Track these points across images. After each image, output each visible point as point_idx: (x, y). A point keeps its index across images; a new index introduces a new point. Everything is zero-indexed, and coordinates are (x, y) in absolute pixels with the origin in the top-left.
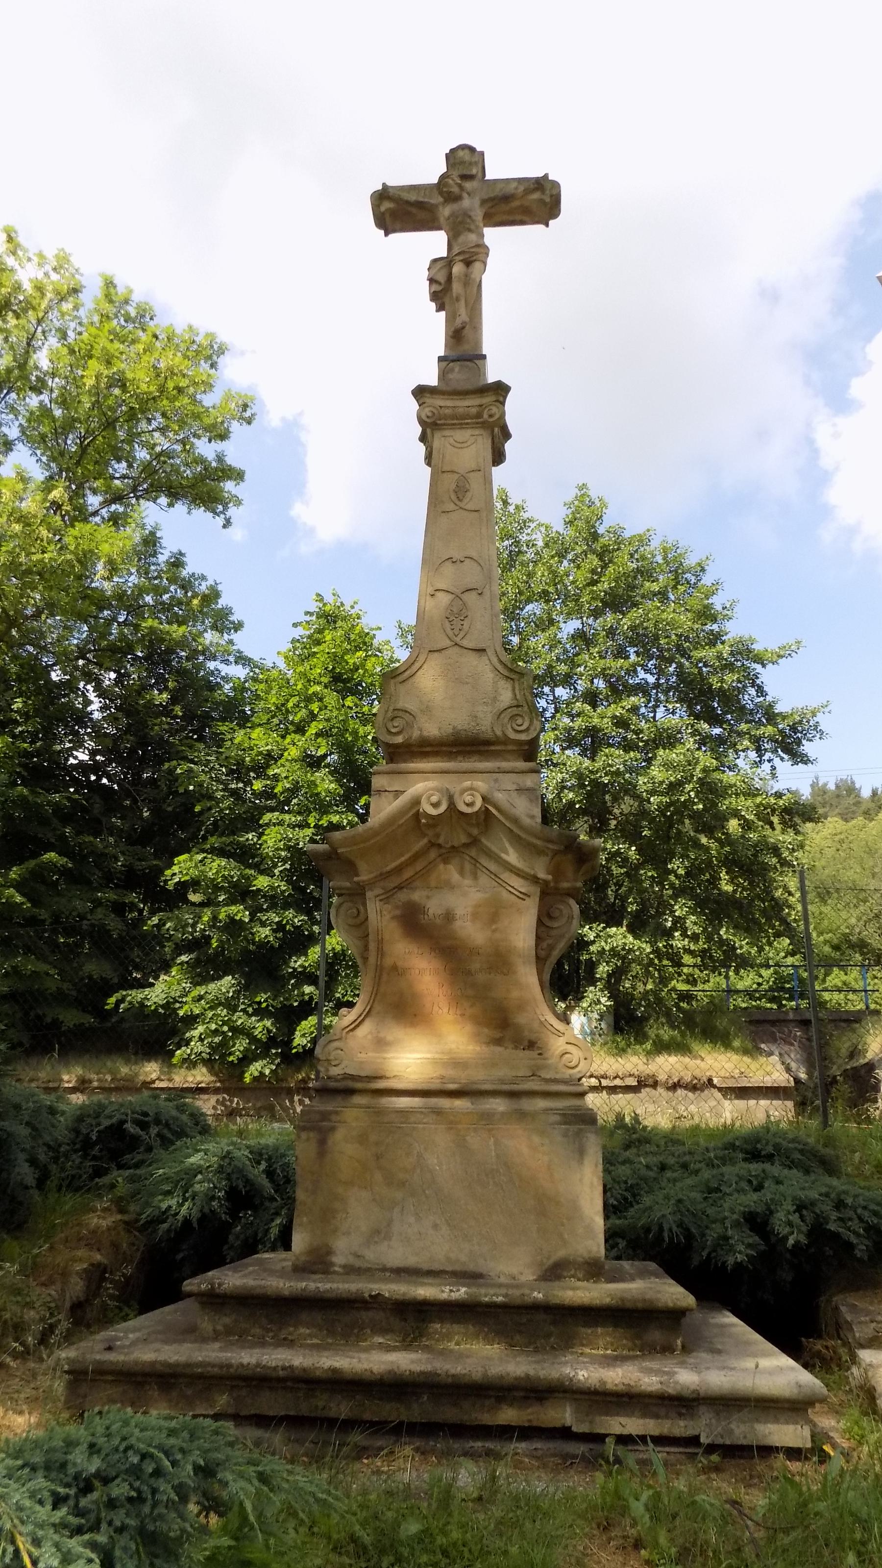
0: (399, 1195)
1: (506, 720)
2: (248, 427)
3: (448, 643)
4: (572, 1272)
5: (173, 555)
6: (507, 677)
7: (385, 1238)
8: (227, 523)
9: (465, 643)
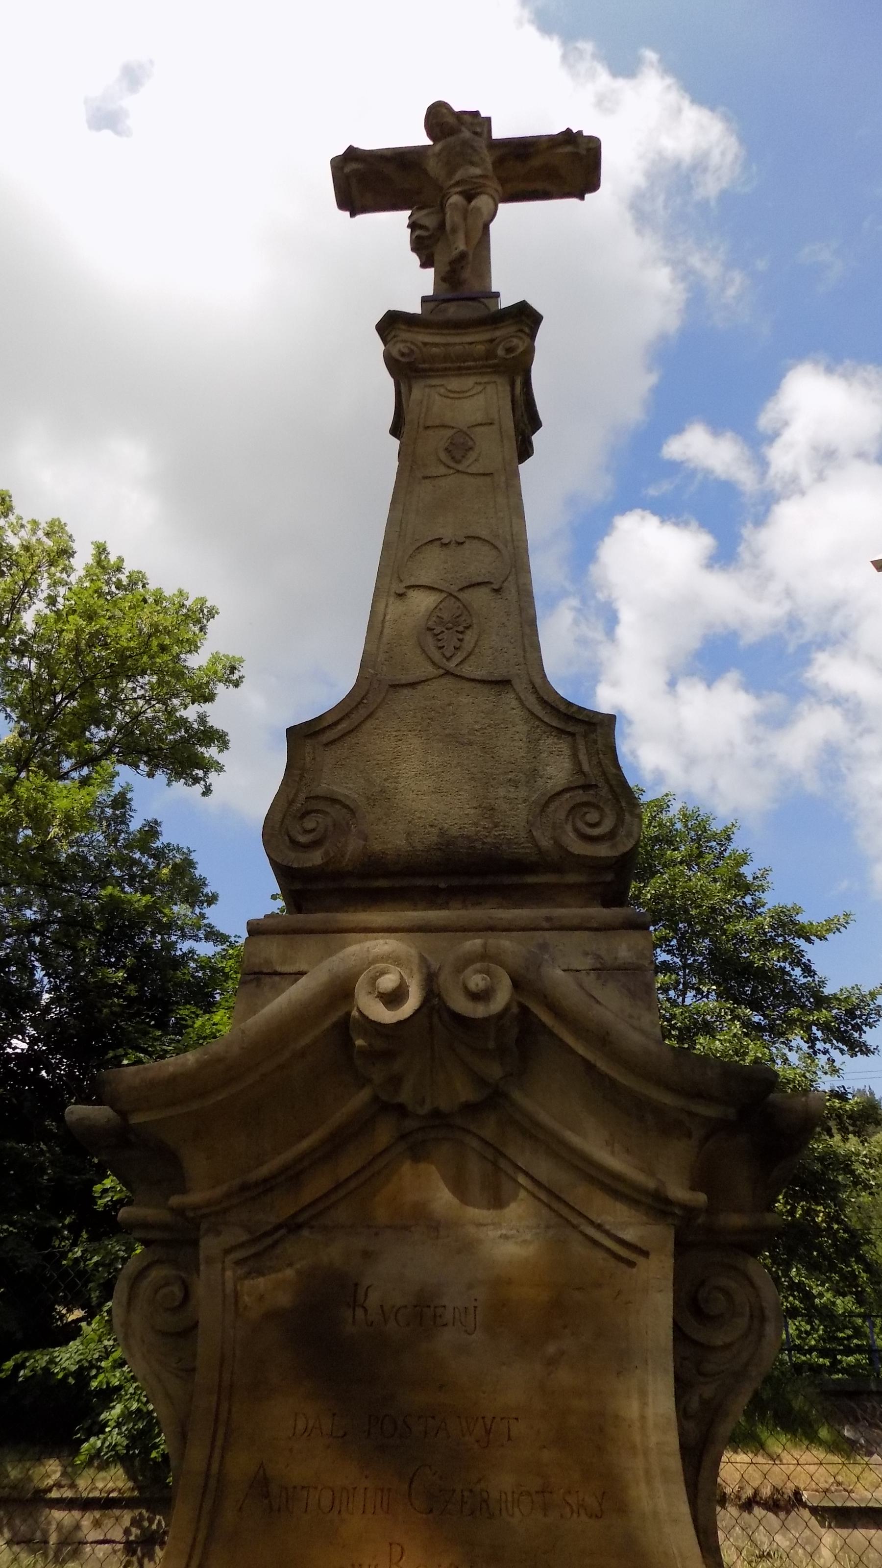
1: (562, 815)
2: (235, 689)
3: (431, 671)
5: (148, 823)
6: (561, 731)
8: (207, 791)
9: (467, 670)
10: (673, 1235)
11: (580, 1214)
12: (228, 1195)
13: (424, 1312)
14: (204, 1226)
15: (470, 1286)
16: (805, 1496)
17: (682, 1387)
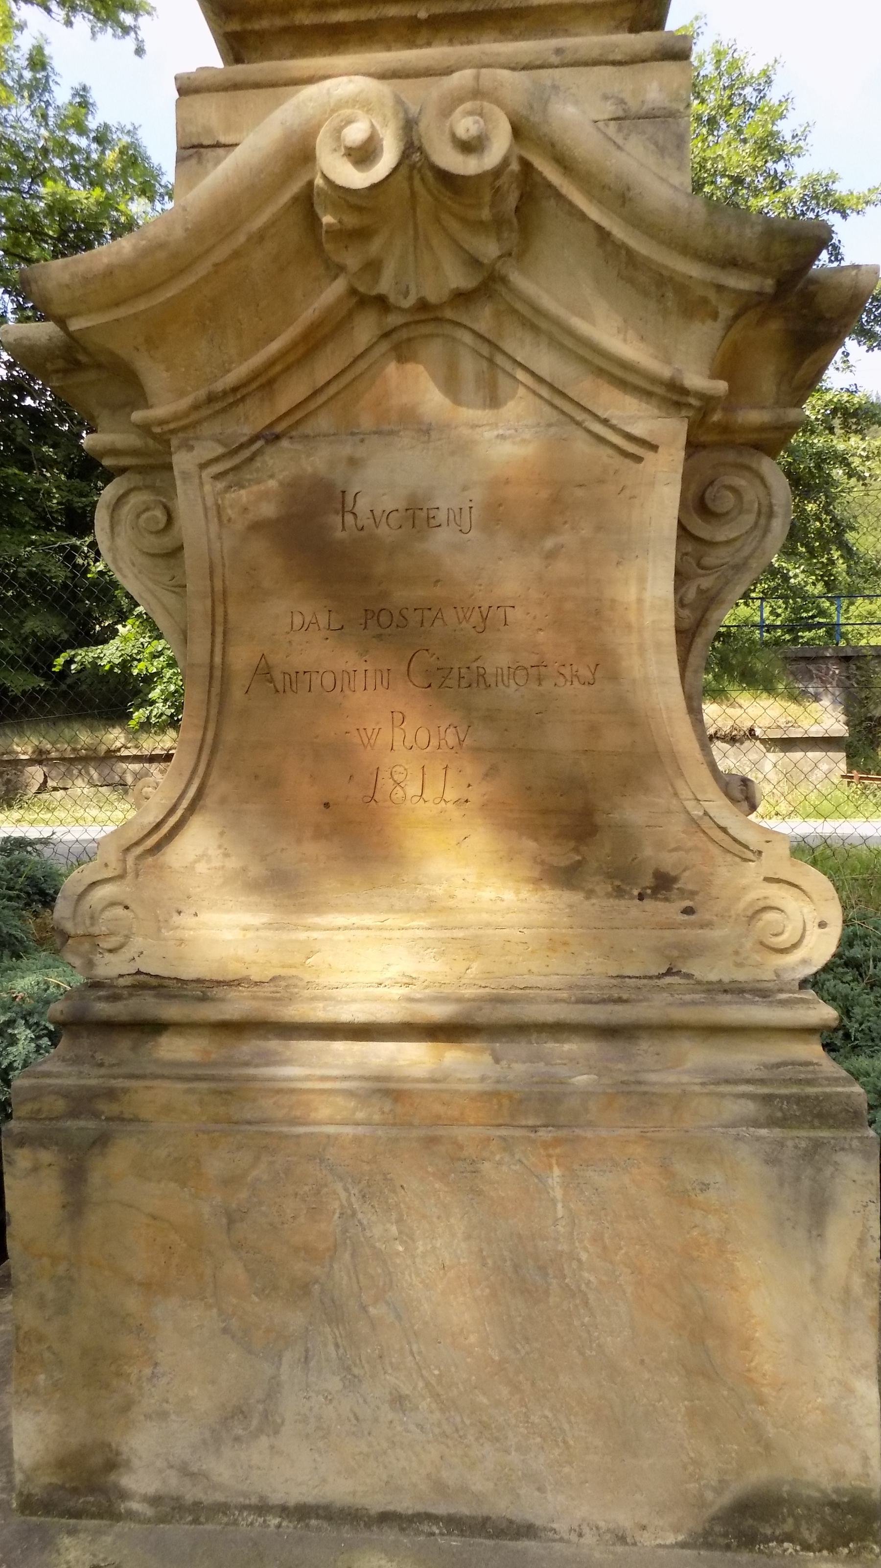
0: (296, 1320)
4: (789, 1526)
7: (260, 1431)
10: (686, 428)
11: (585, 409)
12: (196, 407)
13: (417, 516)
14: (174, 442)
15: (465, 488)
16: (758, 732)
17: (681, 577)
